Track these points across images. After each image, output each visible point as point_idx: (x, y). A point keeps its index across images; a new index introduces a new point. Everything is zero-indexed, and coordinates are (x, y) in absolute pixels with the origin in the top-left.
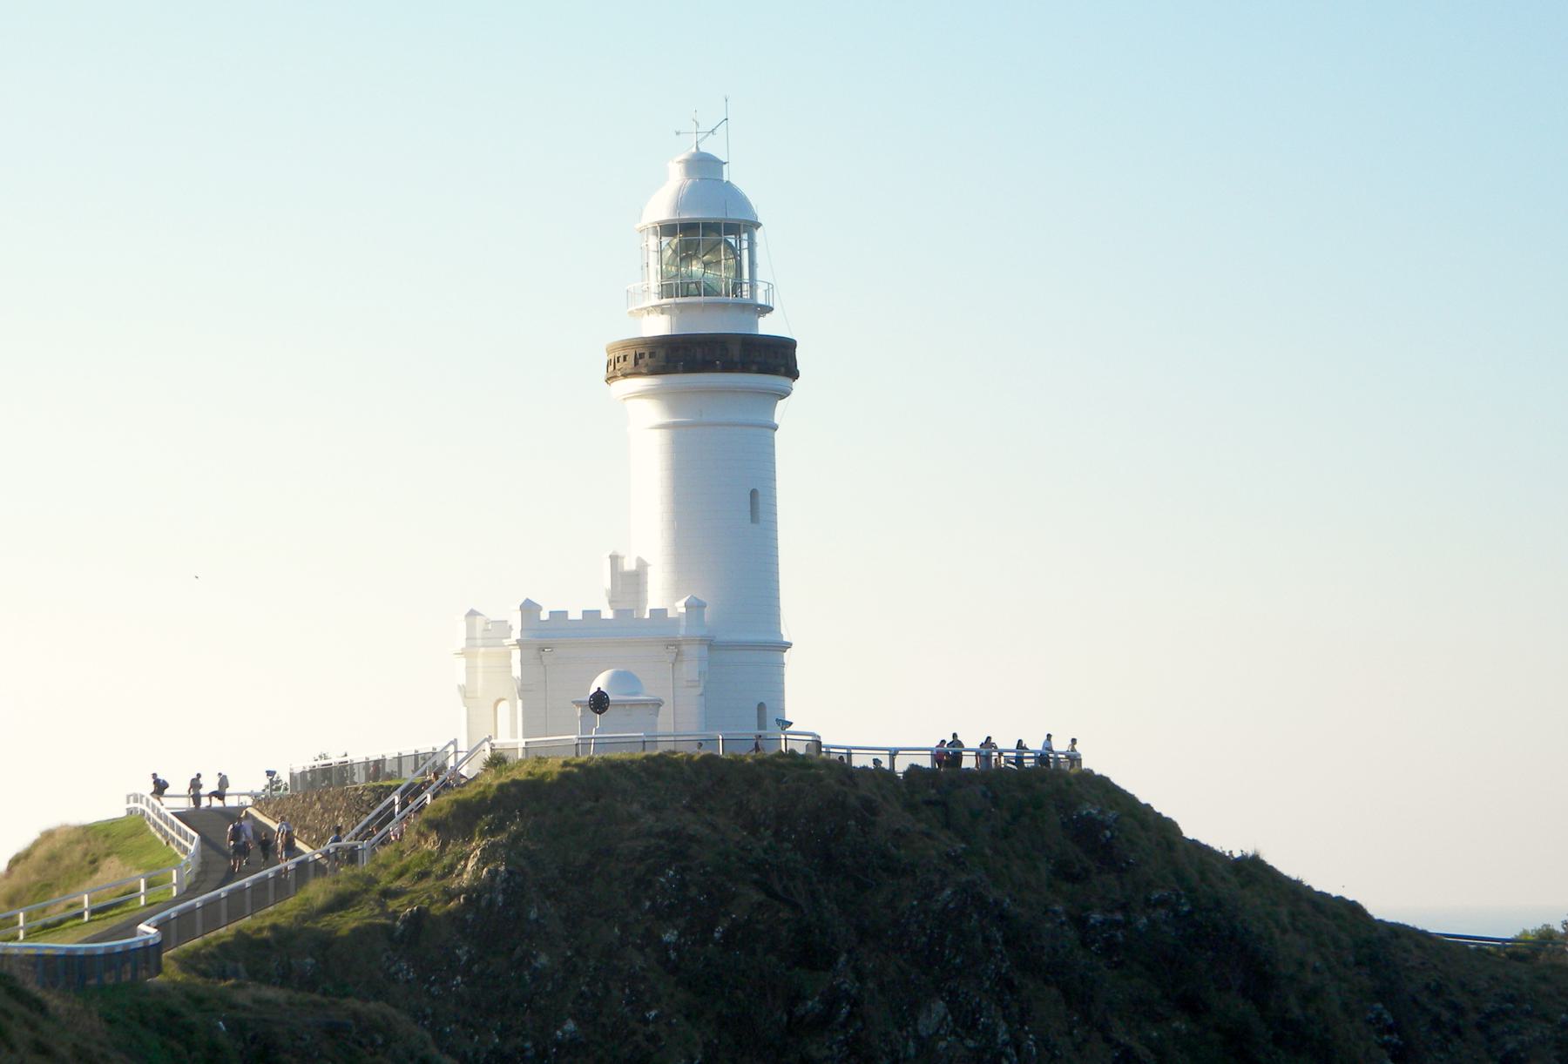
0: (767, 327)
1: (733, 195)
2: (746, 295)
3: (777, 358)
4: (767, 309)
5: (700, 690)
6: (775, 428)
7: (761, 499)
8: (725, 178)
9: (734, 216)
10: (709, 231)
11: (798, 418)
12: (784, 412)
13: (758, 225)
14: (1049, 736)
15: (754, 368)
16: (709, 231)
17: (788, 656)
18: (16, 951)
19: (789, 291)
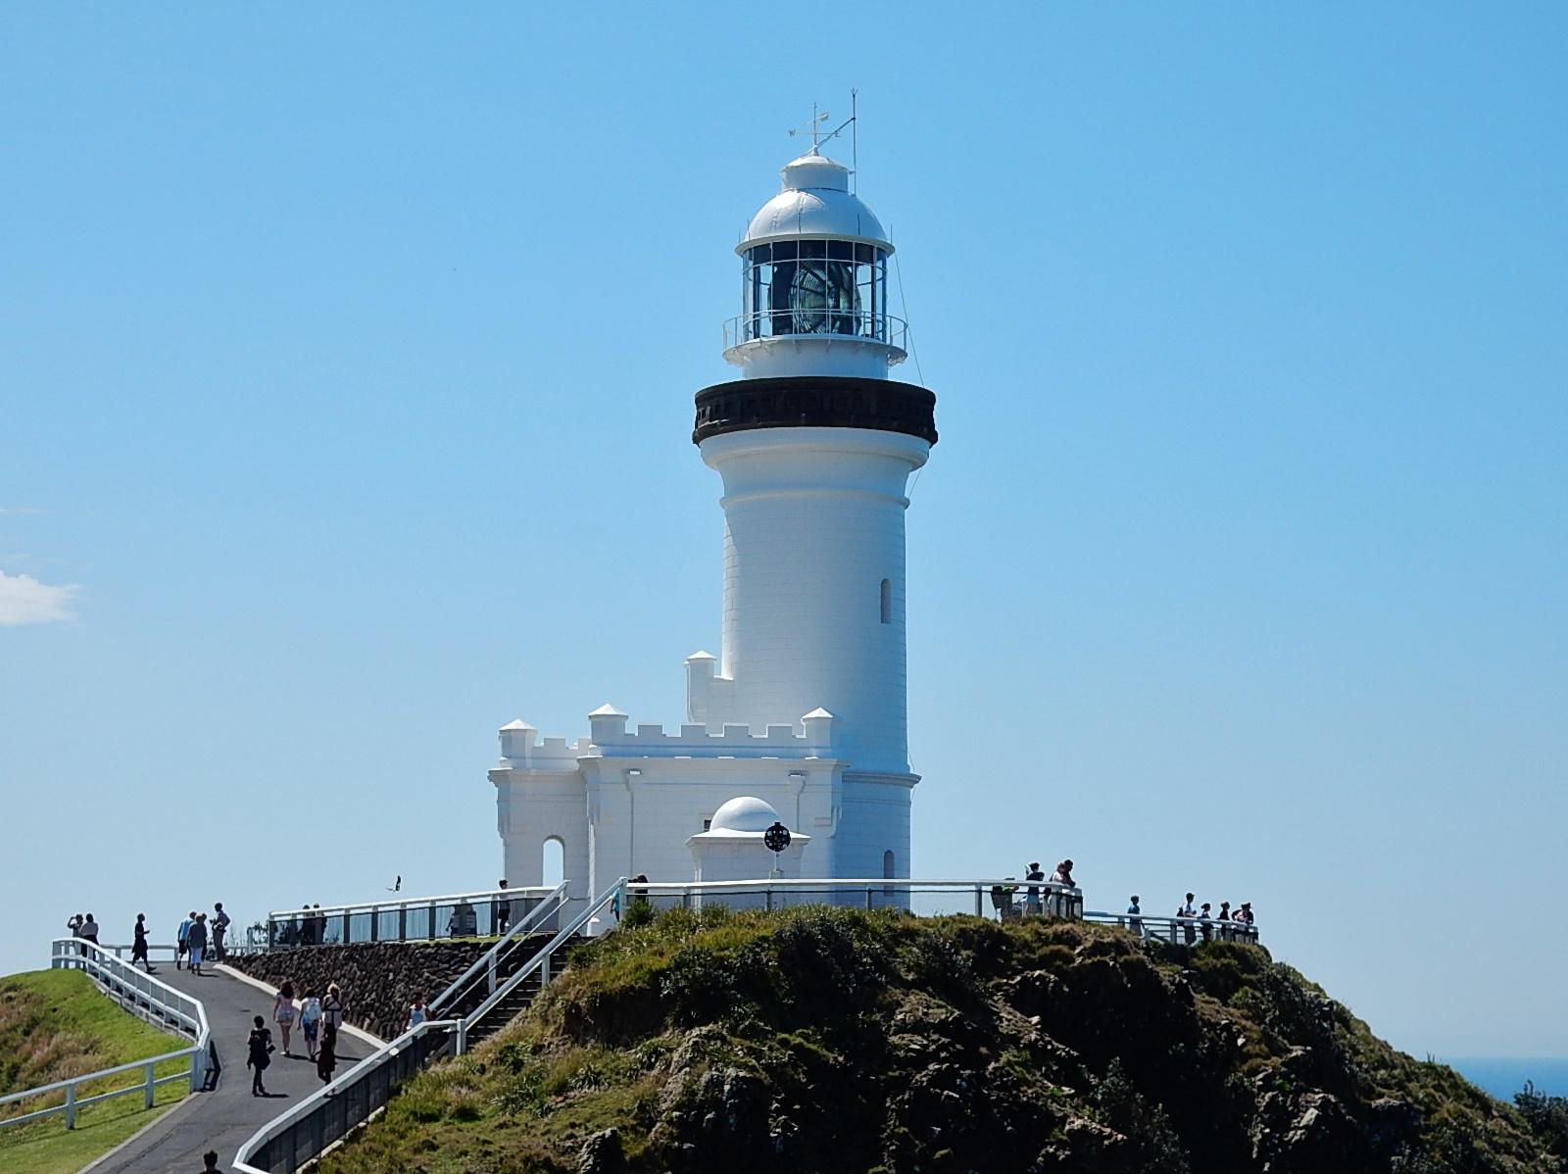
0: (897, 373)
1: (861, 215)
2: (888, 342)
3: (909, 412)
4: (899, 354)
5: (832, 831)
6: (906, 504)
7: (893, 592)
8: (851, 191)
9: (864, 238)
10: (817, 269)
11: (937, 490)
12: (915, 484)
13: (873, 252)
14: (141, 918)
15: (895, 424)
16: (817, 269)
17: (916, 793)
18: (380, 1062)
19: (921, 317)
